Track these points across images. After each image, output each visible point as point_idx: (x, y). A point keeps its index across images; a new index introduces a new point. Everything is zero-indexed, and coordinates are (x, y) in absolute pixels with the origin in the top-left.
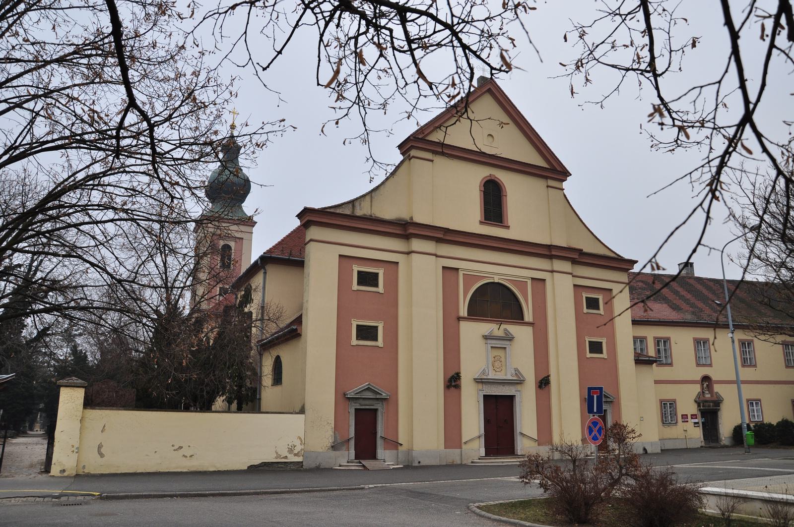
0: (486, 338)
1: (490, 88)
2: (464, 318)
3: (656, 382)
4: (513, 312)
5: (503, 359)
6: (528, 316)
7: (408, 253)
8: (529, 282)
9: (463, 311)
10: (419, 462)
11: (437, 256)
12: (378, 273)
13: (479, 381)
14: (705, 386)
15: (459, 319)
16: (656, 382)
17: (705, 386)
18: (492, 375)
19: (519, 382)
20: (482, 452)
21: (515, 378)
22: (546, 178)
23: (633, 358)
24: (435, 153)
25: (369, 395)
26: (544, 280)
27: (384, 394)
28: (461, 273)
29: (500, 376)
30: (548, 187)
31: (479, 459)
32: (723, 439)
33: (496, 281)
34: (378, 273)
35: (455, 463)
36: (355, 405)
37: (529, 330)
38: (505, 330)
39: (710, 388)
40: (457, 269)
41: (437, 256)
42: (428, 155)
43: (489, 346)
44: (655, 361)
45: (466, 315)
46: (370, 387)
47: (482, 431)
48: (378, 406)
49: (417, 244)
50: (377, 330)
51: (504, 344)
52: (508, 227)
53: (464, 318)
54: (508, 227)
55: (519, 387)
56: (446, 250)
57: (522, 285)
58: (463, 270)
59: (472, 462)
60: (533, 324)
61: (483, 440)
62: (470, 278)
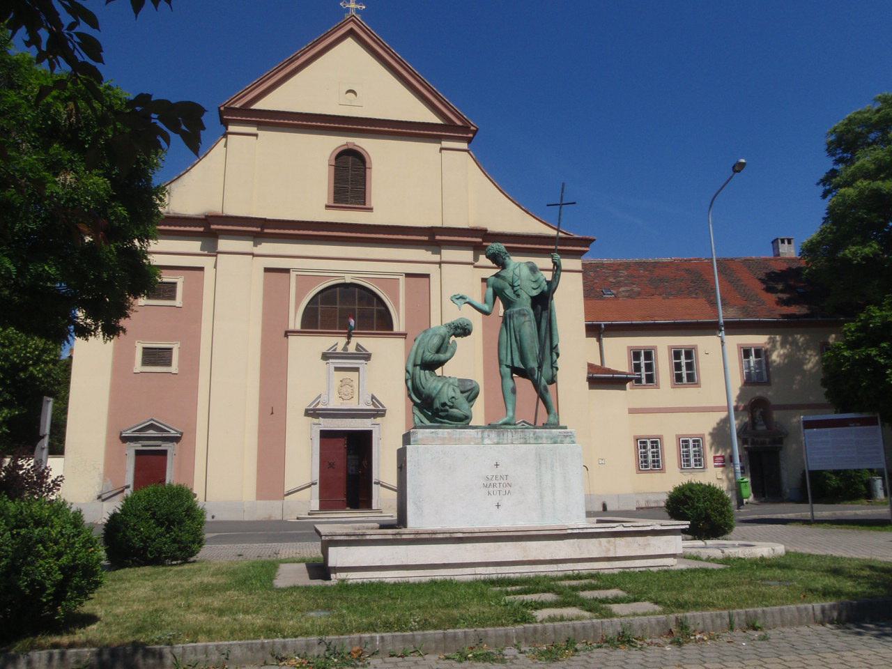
0: (326, 356)
1: (352, 29)
2: (294, 332)
3: (632, 411)
4: (378, 319)
5: (355, 384)
6: (399, 325)
7: (440, 263)
8: (402, 279)
9: (295, 322)
10: (213, 517)
11: (253, 255)
12: (175, 283)
13: (312, 413)
14: (758, 413)
15: (287, 333)
16: (632, 411)
17: (758, 413)
18: (335, 403)
19: (378, 413)
20: (315, 505)
21: (372, 407)
22: (437, 139)
23: (585, 375)
24: (260, 125)
25: (151, 433)
26: (427, 276)
27: (173, 432)
28: (293, 274)
29: (353, 404)
30: (442, 149)
31: (309, 514)
32: (788, 491)
33: (348, 280)
34: (175, 283)
35: (273, 519)
36: (136, 445)
37: (400, 342)
38: (358, 345)
39: (766, 417)
40: (287, 271)
41: (253, 255)
42: (253, 130)
43: (332, 367)
44: (630, 380)
45: (298, 327)
46: (154, 423)
47: (316, 477)
48: (165, 446)
49: (448, 254)
50: (171, 353)
51: (357, 363)
52: (370, 209)
53: (294, 332)
54: (370, 209)
55: (378, 420)
56: (266, 247)
57: (391, 283)
58: (296, 270)
59: (298, 519)
60: (405, 335)
61: (316, 489)
62: (305, 279)
